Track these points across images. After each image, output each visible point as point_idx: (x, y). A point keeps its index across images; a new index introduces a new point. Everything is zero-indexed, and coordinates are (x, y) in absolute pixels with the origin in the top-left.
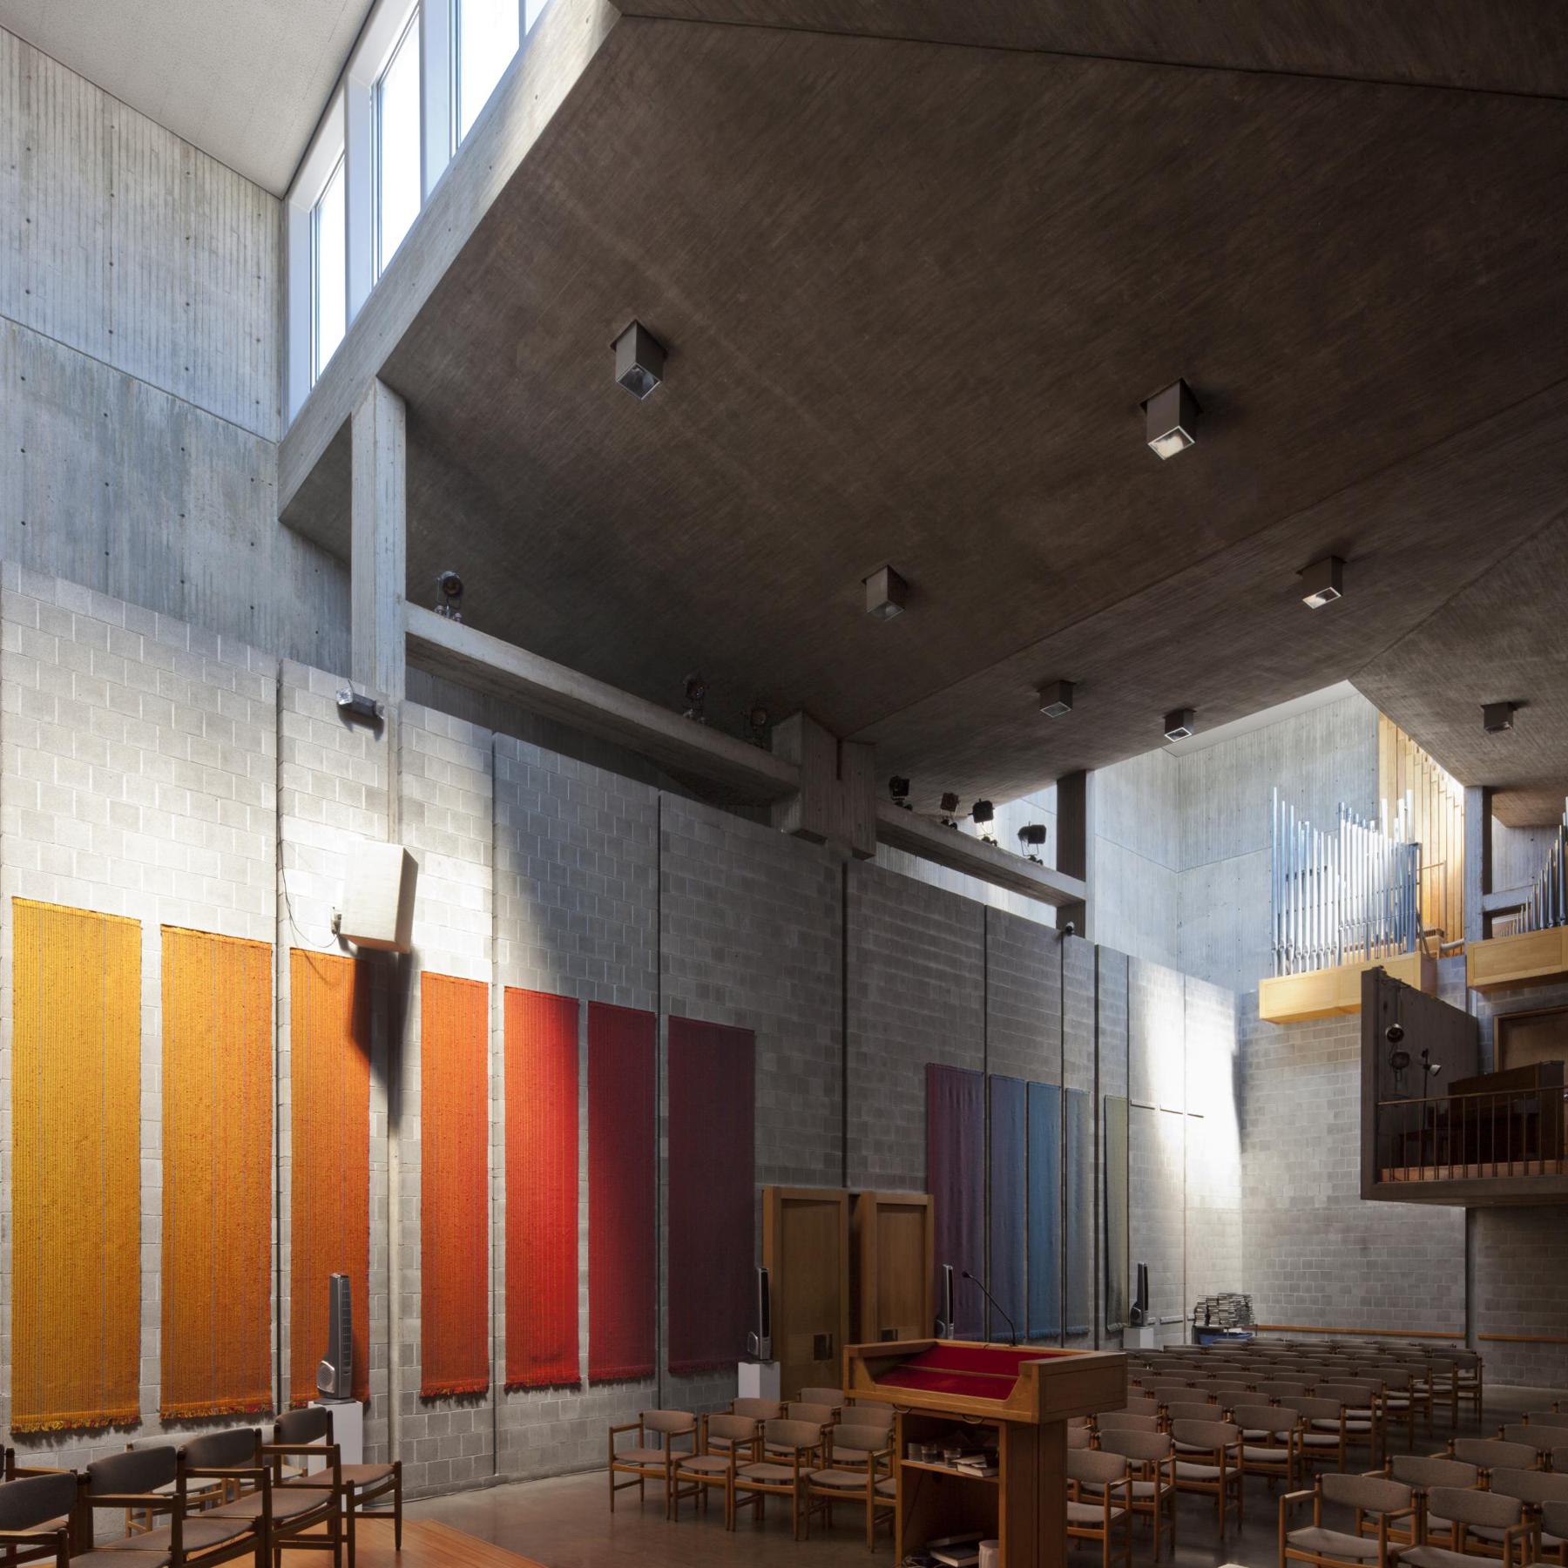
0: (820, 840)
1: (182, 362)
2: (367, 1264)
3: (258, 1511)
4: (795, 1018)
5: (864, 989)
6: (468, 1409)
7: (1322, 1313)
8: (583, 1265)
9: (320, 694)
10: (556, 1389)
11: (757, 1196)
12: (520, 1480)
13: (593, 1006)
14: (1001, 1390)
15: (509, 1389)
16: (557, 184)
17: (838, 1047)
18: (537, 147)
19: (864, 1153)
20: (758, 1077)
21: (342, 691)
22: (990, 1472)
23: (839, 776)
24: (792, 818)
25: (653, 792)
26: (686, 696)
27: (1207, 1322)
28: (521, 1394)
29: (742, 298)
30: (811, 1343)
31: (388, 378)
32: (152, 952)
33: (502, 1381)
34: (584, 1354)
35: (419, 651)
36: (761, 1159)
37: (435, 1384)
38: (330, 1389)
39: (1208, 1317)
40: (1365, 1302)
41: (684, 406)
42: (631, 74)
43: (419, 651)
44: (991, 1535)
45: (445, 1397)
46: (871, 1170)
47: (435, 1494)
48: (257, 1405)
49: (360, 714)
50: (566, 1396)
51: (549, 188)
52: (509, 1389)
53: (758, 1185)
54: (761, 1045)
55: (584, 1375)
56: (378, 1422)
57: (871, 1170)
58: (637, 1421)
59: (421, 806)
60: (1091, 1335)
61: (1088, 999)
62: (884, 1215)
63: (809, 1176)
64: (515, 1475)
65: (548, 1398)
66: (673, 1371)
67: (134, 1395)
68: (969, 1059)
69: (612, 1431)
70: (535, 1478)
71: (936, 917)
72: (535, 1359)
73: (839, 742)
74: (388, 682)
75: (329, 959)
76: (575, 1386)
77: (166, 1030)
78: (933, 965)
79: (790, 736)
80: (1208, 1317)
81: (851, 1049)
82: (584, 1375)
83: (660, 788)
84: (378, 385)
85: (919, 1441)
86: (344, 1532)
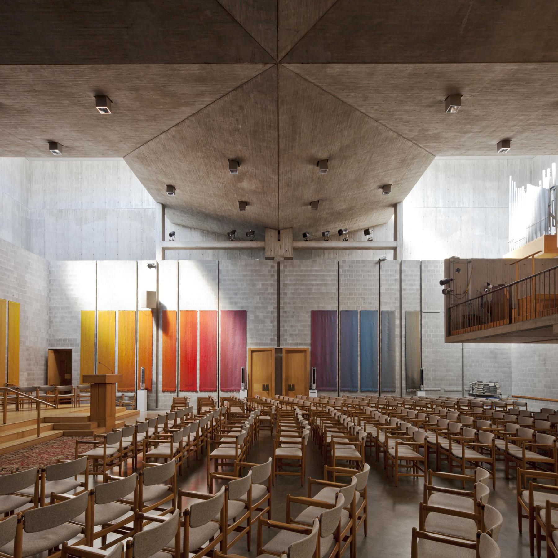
4: (260, 305)
5: (286, 294)
7: (533, 391)
14: (71, 393)
19: (285, 337)
23: (279, 240)
27: (473, 392)
30: (261, 387)
34: (198, 385)
36: (466, 345)
39: (473, 390)
40: (546, 387)
54: (248, 314)
55: (198, 390)
56: (153, 395)
57: (288, 342)
60: (378, 392)
61: (396, 280)
62: (290, 355)
66: (222, 391)
68: (331, 306)
71: (316, 269)
73: (279, 233)
76: (196, 391)
78: (314, 283)
80: (473, 390)
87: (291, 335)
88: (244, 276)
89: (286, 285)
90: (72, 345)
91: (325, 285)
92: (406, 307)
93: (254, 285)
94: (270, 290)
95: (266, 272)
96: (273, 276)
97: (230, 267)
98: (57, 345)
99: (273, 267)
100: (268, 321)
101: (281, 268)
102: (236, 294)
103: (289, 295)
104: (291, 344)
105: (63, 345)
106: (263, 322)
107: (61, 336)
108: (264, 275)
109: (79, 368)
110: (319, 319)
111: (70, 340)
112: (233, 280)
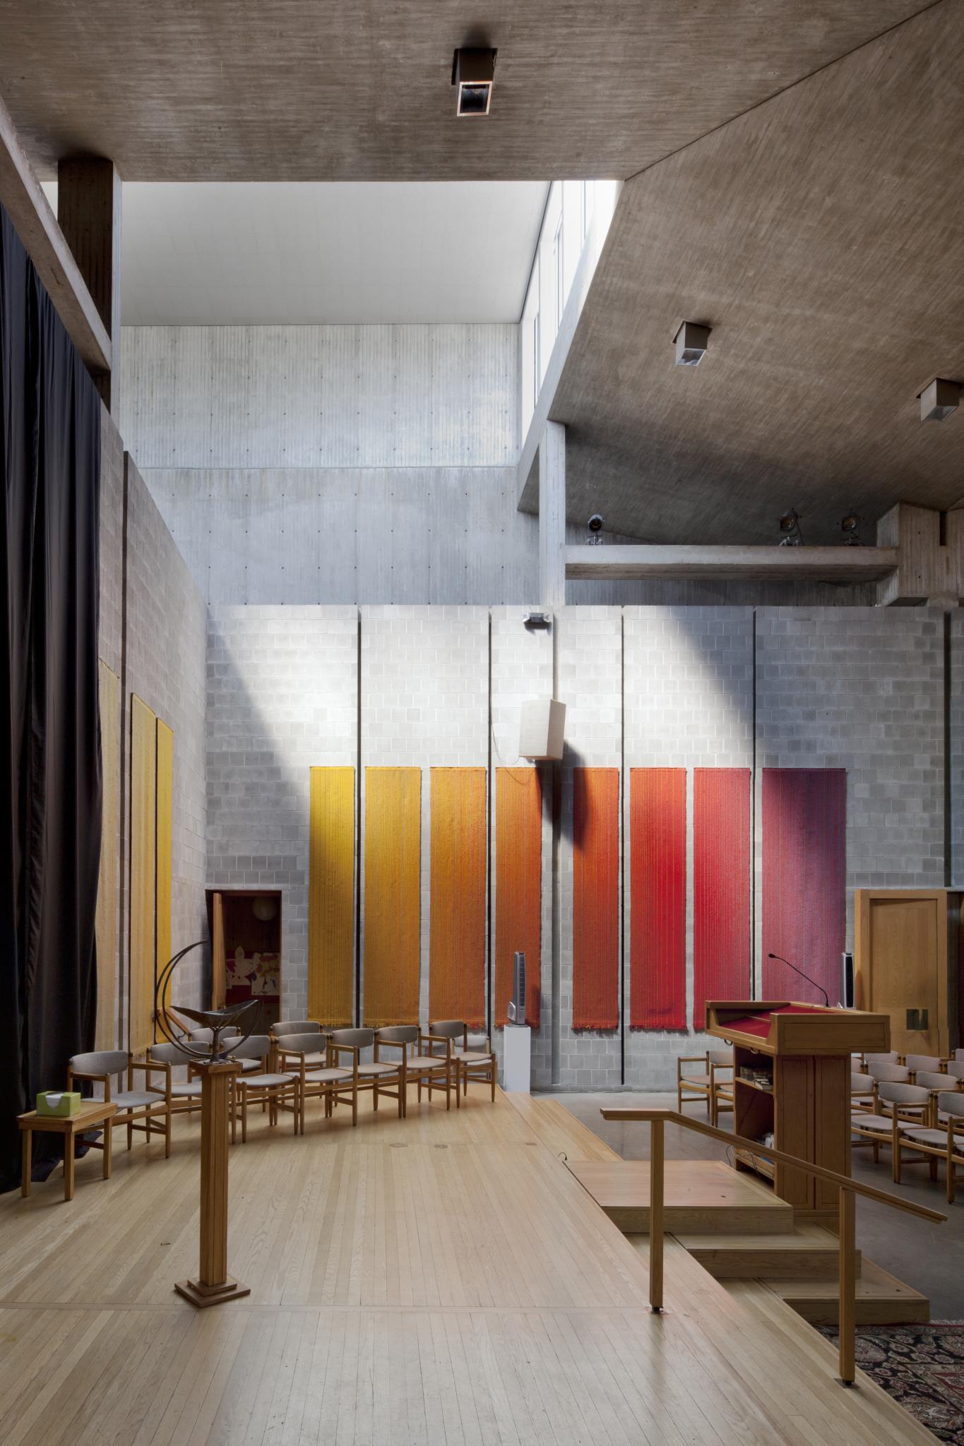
0: (921, 602)
1: (466, 446)
2: (540, 947)
3: (401, 1063)
4: (890, 752)
6: (606, 1039)
8: (690, 949)
9: (513, 617)
10: (669, 1031)
11: (848, 897)
12: (640, 1091)
13: (699, 772)
15: (632, 1028)
16: (615, 280)
17: (941, 769)
18: (598, 268)
20: (850, 805)
21: (525, 612)
22: (769, 1088)
24: (892, 591)
25: (749, 610)
26: (787, 527)
28: (642, 1033)
29: (751, 274)
31: (553, 419)
32: (427, 783)
33: (627, 1023)
35: (574, 572)
37: (582, 1021)
38: (513, 1018)
41: (732, 351)
42: (639, 204)
43: (574, 572)
44: (772, 1132)
47: (581, 1091)
48: (477, 1024)
49: (535, 624)
50: (676, 1037)
51: (611, 283)
52: (632, 1028)
53: (848, 888)
55: (690, 1025)
58: (705, 1056)
59: (574, 667)
63: (907, 879)
64: (637, 1087)
65: (663, 1037)
67: (417, 1013)
69: (680, 1060)
70: (652, 1091)
72: (652, 1012)
74: (553, 602)
75: (520, 770)
76: (684, 1031)
77: (432, 823)
79: (889, 526)
82: (690, 1025)
83: (754, 604)
84: (549, 425)
85: (746, 1066)
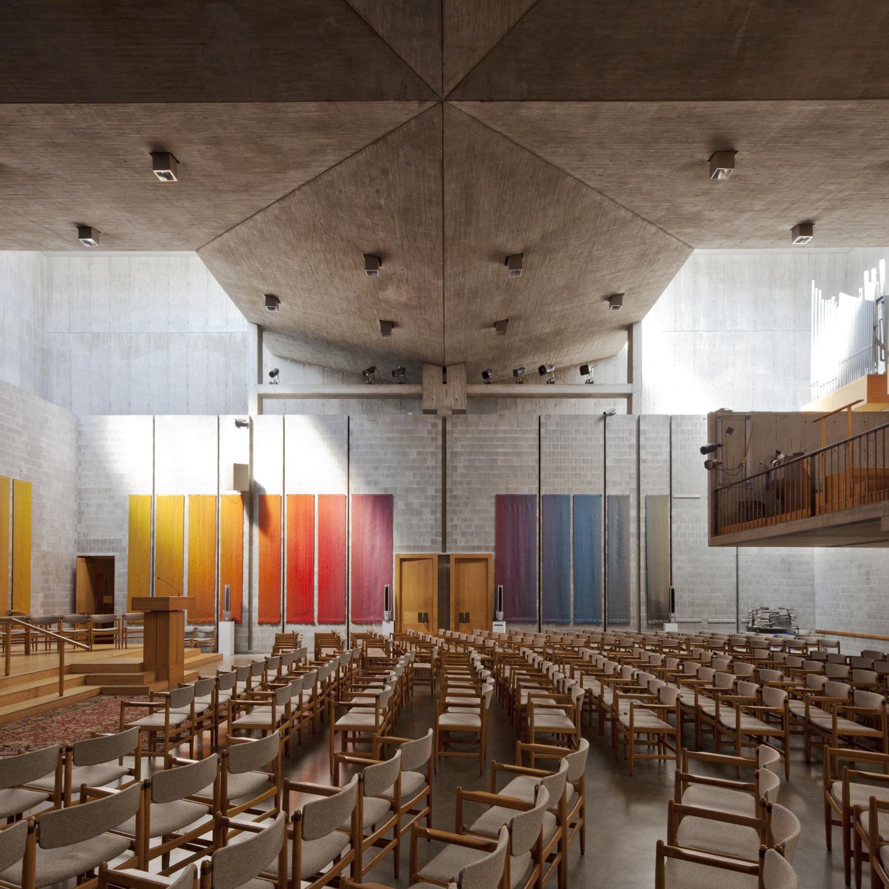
4: (415, 486)
5: (455, 468)
14: (113, 626)
15: (288, 622)
19: (455, 537)
23: (445, 382)
27: (753, 624)
30: (416, 616)
34: (316, 614)
39: (753, 621)
45: (267, 623)
46: (459, 544)
54: (395, 500)
55: (316, 621)
56: (244, 629)
57: (459, 544)
60: (603, 625)
62: (461, 565)
66: (353, 622)
68: (527, 488)
71: (503, 428)
73: (444, 371)
76: (313, 624)
78: (500, 450)
80: (753, 621)
81: (448, 495)
86: (852, 859)
87: (464, 534)
88: (389, 439)
89: (455, 454)
90: (114, 550)
91: (519, 454)
92: (647, 490)
93: (405, 454)
94: (431, 462)
95: (424, 434)
96: (434, 439)
97: (367, 425)
98: (91, 550)
99: (434, 425)
100: (427, 511)
101: (448, 428)
102: (376, 469)
103: (461, 470)
104: (464, 548)
105: (101, 550)
106: (419, 513)
107: (96, 535)
108: (421, 439)
109: (126, 587)
110: (509, 508)
111: (111, 542)
112: (371, 446)
